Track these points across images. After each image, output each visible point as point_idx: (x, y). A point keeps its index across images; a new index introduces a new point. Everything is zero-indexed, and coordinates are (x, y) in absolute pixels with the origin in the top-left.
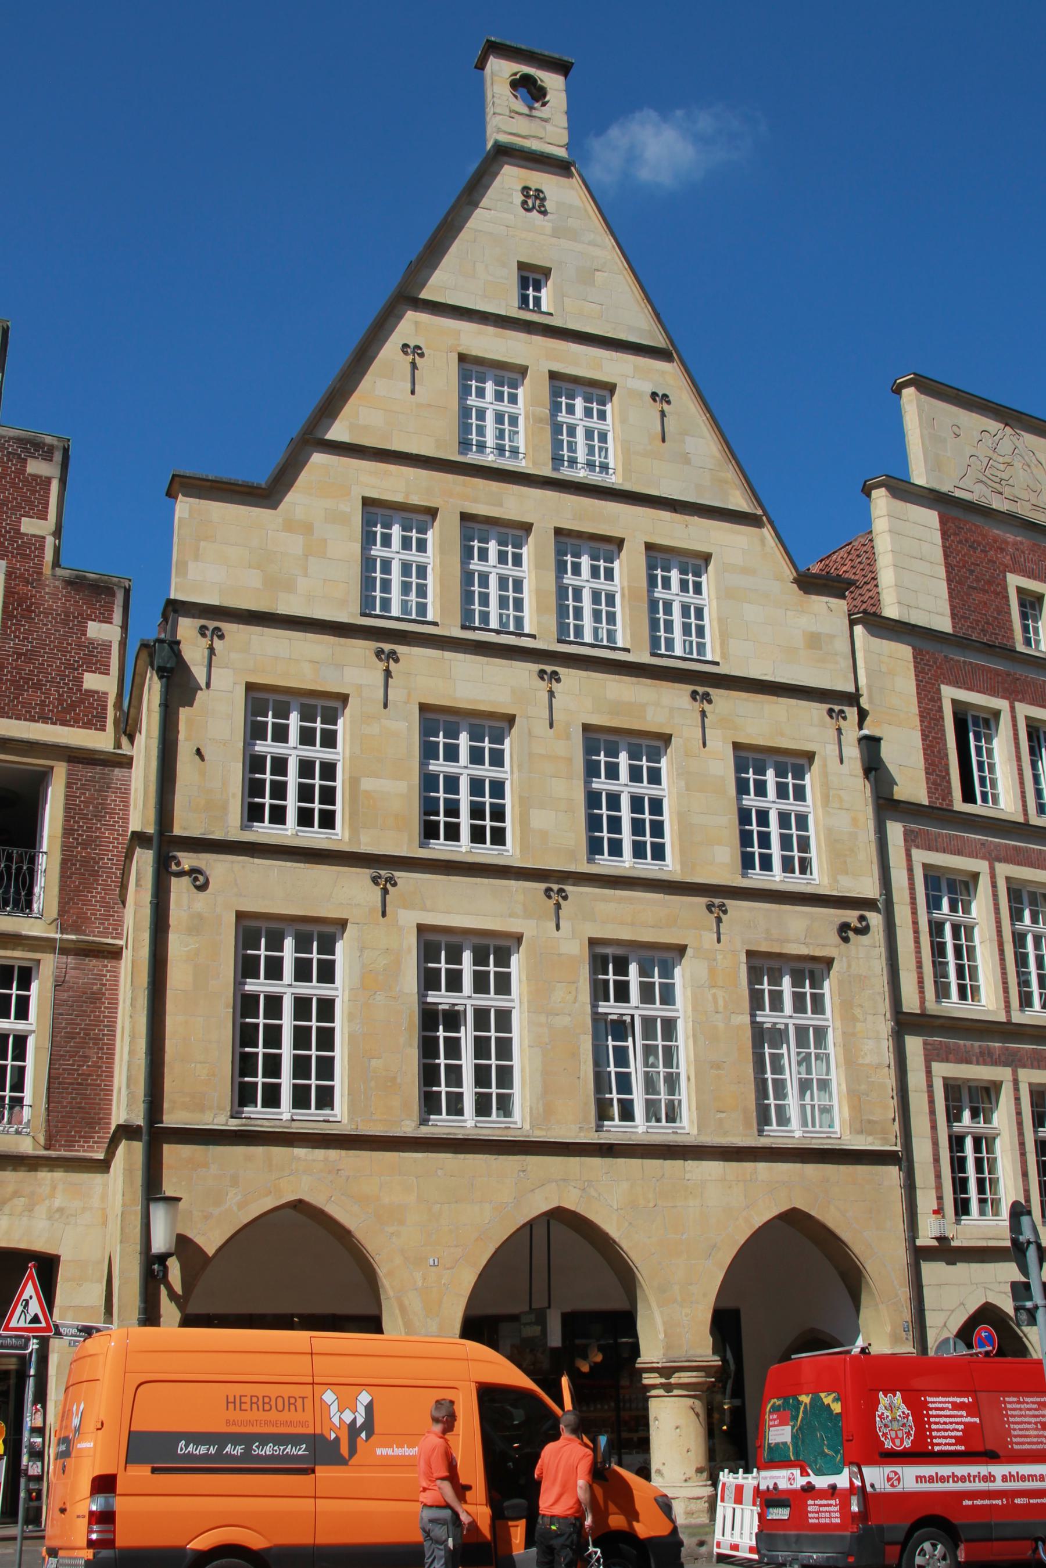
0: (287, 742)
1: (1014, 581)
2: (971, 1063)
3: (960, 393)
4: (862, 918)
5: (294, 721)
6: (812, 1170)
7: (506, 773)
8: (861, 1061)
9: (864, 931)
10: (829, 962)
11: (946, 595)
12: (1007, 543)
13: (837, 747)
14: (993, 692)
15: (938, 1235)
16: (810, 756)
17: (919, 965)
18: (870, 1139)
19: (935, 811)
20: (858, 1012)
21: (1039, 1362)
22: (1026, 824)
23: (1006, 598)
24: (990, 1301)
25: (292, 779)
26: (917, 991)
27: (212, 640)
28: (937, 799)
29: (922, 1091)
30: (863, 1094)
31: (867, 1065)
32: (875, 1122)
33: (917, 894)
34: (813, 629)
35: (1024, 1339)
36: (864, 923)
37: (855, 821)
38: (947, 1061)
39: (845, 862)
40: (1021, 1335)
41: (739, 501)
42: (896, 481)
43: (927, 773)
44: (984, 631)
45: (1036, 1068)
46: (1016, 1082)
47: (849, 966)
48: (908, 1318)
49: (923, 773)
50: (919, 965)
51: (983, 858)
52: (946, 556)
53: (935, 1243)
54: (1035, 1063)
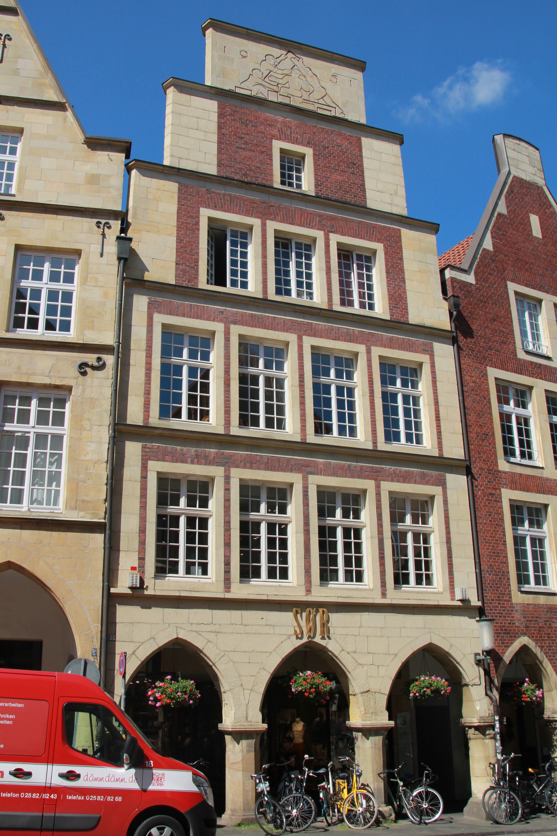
0: (41, 280)
1: (277, 145)
2: (186, 463)
3: (249, 31)
4: (99, 359)
5: (47, 268)
6: (28, 534)
7: (75, 287)
8: (83, 458)
9: (102, 367)
10: (69, 389)
11: (216, 152)
12: (277, 121)
13: (100, 247)
14: (248, 213)
15: (130, 585)
16: (78, 253)
17: (147, 393)
18: (82, 514)
19: (177, 288)
20: (86, 424)
21: (550, 722)
22: (265, 300)
23: (270, 156)
24: (180, 636)
25: (43, 303)
26: (143, 411)
27: (104, 229)
28: (185, 281)
29: (136, 481)
30: (81, 481)
31: (87, 460)
32: (88, 502)
33: (153, 344)
34: (95, 172)
35: (214, 667)
36: (101, 363)
37: (106, 295)
38: (164, 460)
39: (93, 321)
40: (211, 664)
41: (52, 95)
42: (182, 82)
43: (177, 264)
44: (245, 175)
45: (248, 468)
46: (227, 478)
47: (84, 391)
48: (98, 646)
49: (174, 264)
50: (147, 393)
51: (220, 321)
52: (220, 128)
53: (129, 591)
54: (248, 465)
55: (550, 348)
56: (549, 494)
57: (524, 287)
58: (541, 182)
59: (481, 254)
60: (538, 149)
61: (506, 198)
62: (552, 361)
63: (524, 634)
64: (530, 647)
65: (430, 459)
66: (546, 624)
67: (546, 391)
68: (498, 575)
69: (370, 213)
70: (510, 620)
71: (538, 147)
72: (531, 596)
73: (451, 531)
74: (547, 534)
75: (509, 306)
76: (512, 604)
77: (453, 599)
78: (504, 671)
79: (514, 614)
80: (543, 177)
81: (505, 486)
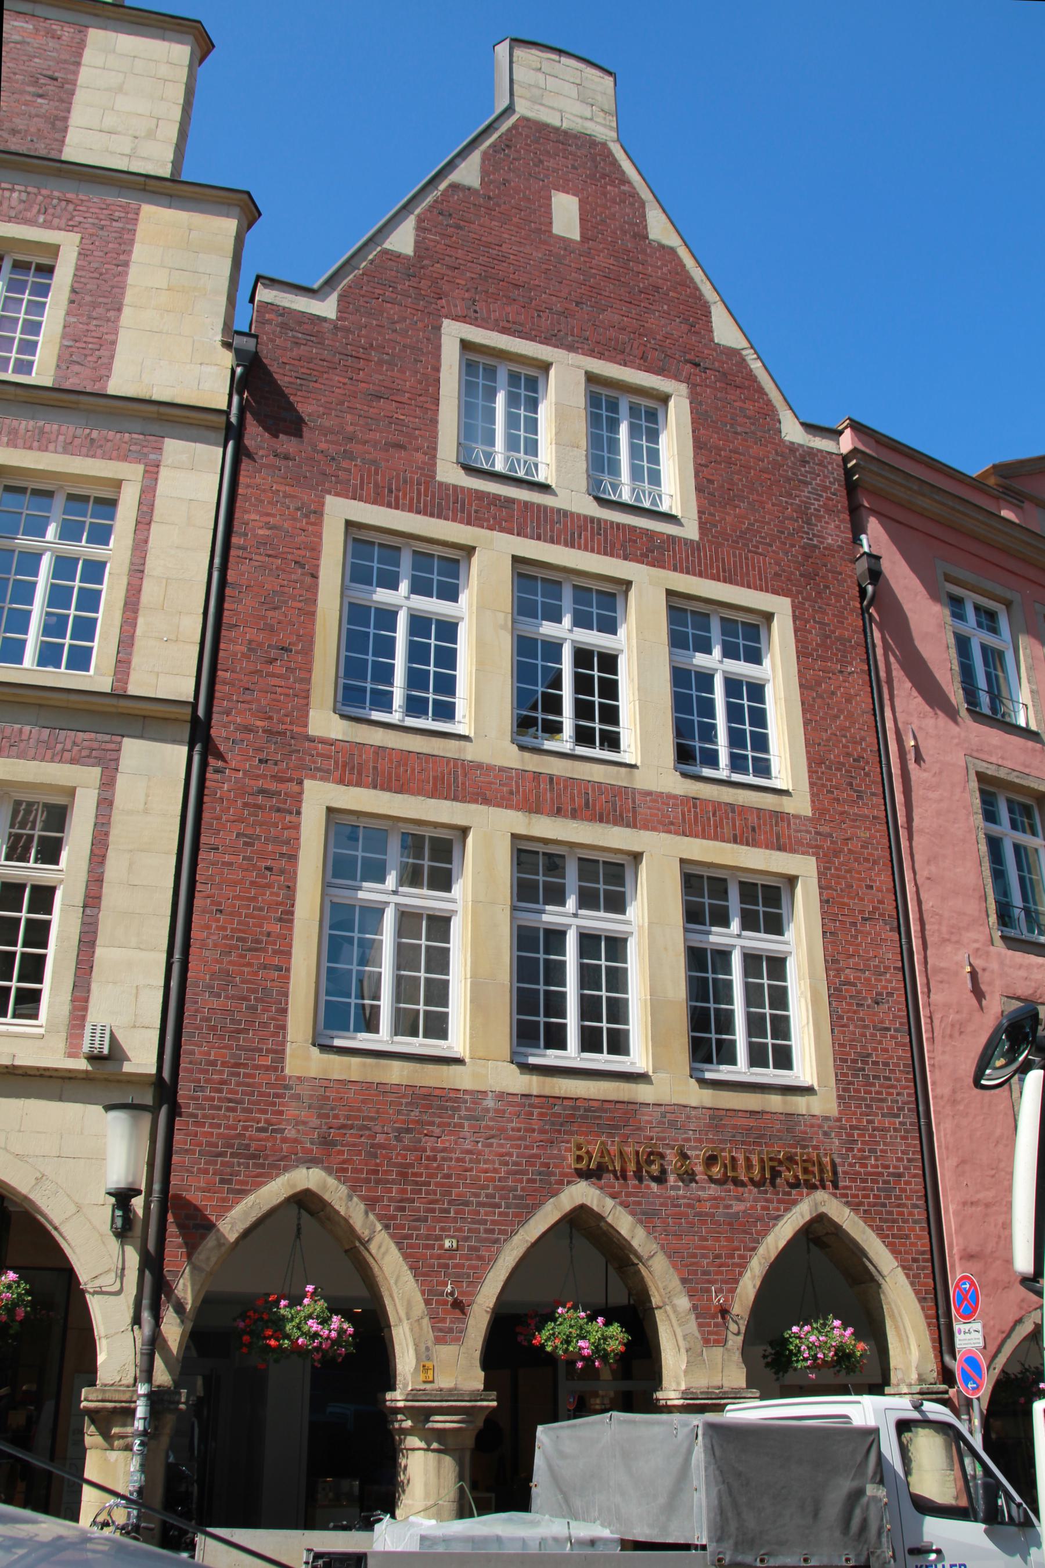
55: (553, 467)
56: (476, 801)
57: (495, 335)
58: (603, 130)
59: (372, 262)
60: (610, 73)
61: (485, 156)
62: (556, 495)
63: (312, 1162)
64: (327, 1197)
65: (73, 697)
66: (398, 1139)
67: (670, 593)
68: (246, 999)
69: (60, 170)
70: (267, 1121)
71: (612, 70)
72: (355, 1061)
73: (107, 877)
74: (459, 907)
75: (437, 369)
76: (284, 1078)
77: (71, 1055)
78: (213, 1260)
79: (281, 1104)
80: (614, 125)
81: (319, 774)
